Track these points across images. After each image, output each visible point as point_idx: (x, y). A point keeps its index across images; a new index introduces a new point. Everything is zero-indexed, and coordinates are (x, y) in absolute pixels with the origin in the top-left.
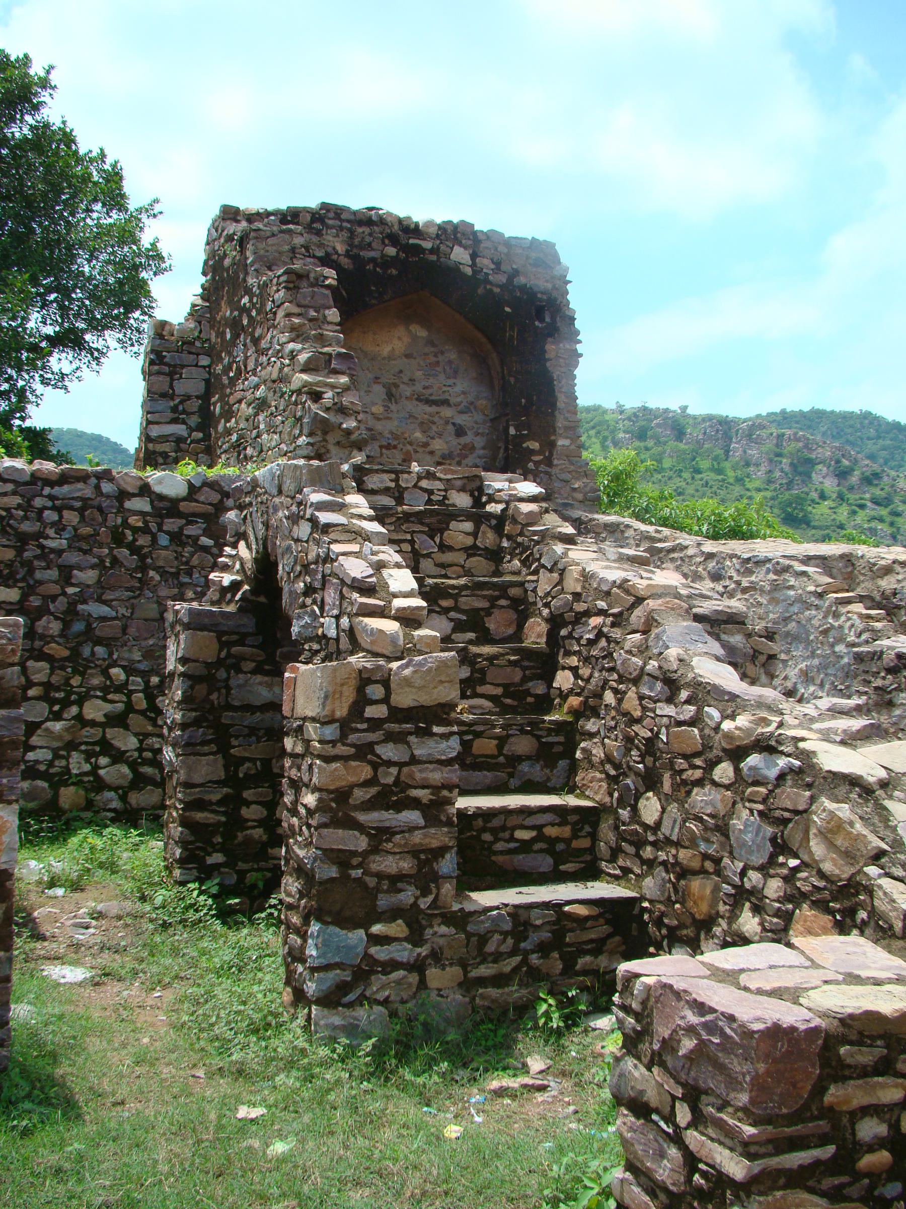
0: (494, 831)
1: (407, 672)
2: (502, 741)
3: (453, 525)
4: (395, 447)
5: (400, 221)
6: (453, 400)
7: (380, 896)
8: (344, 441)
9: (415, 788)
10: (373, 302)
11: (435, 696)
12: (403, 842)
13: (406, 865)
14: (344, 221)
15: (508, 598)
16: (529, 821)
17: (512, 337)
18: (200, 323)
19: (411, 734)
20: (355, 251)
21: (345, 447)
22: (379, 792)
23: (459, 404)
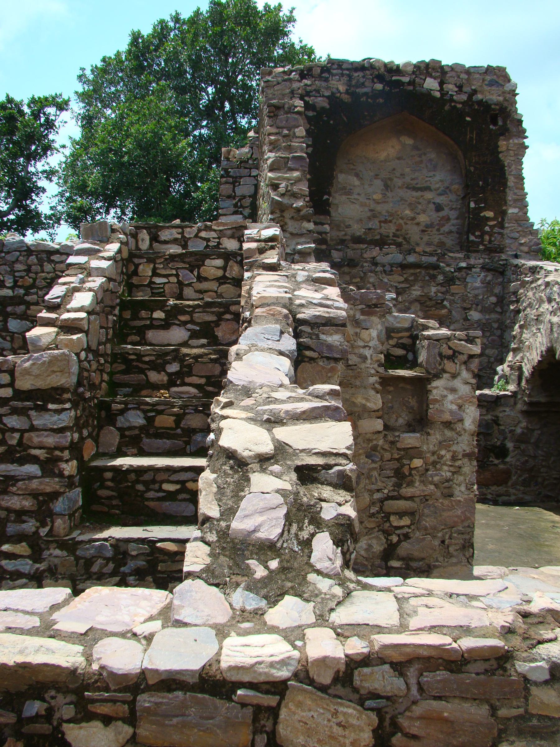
0: (146, 483)
1: (27, 364)
2: (179, 418)
3: (207, 262)
4: (390, 221)
5: (385, 65)
6: (433, 187)
7: (9, 524)
8: (296, 216)
9: (35, 448)
10: (366, 123)
11: (48, 382)
12: (24, 487)
13: (28, 503)
14: (344, 70)
15: (231, 313)
16: (174, 477)
17: (471, 138)
18: (252, 148)
19: (31, 409)
20: (352, 89)
21: (299, 220)
22: (6, 451)
23: (438, 189)
